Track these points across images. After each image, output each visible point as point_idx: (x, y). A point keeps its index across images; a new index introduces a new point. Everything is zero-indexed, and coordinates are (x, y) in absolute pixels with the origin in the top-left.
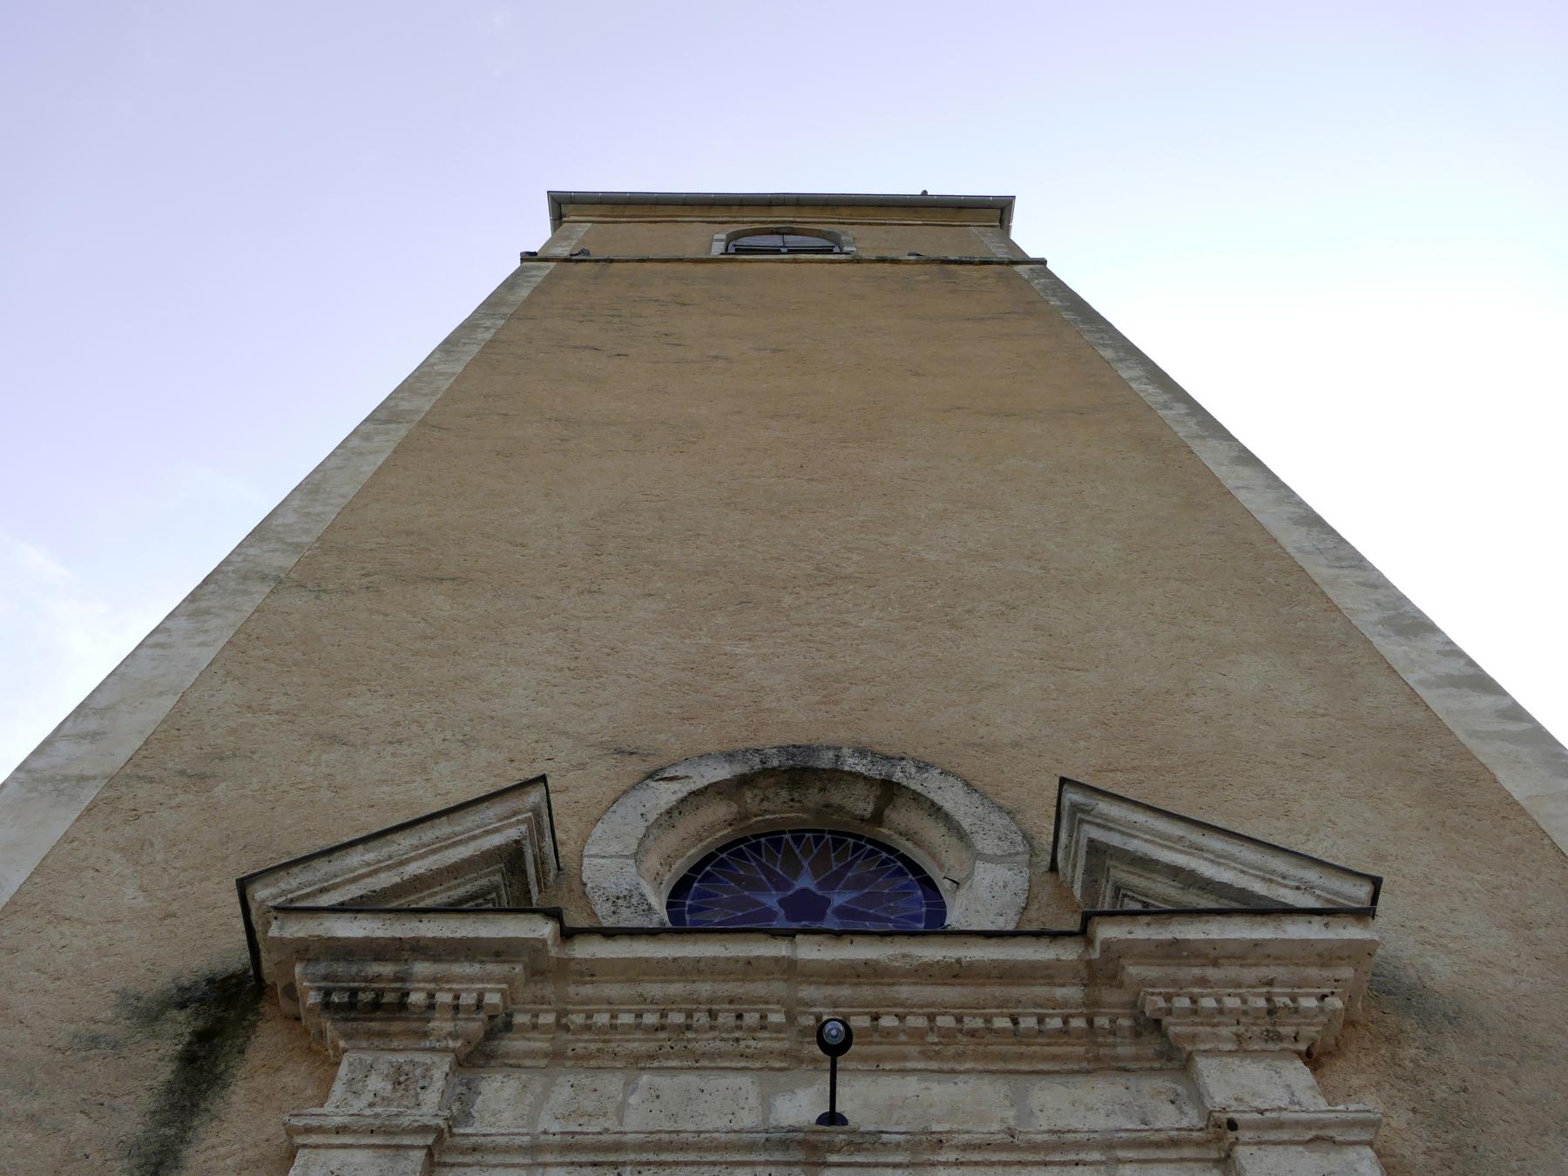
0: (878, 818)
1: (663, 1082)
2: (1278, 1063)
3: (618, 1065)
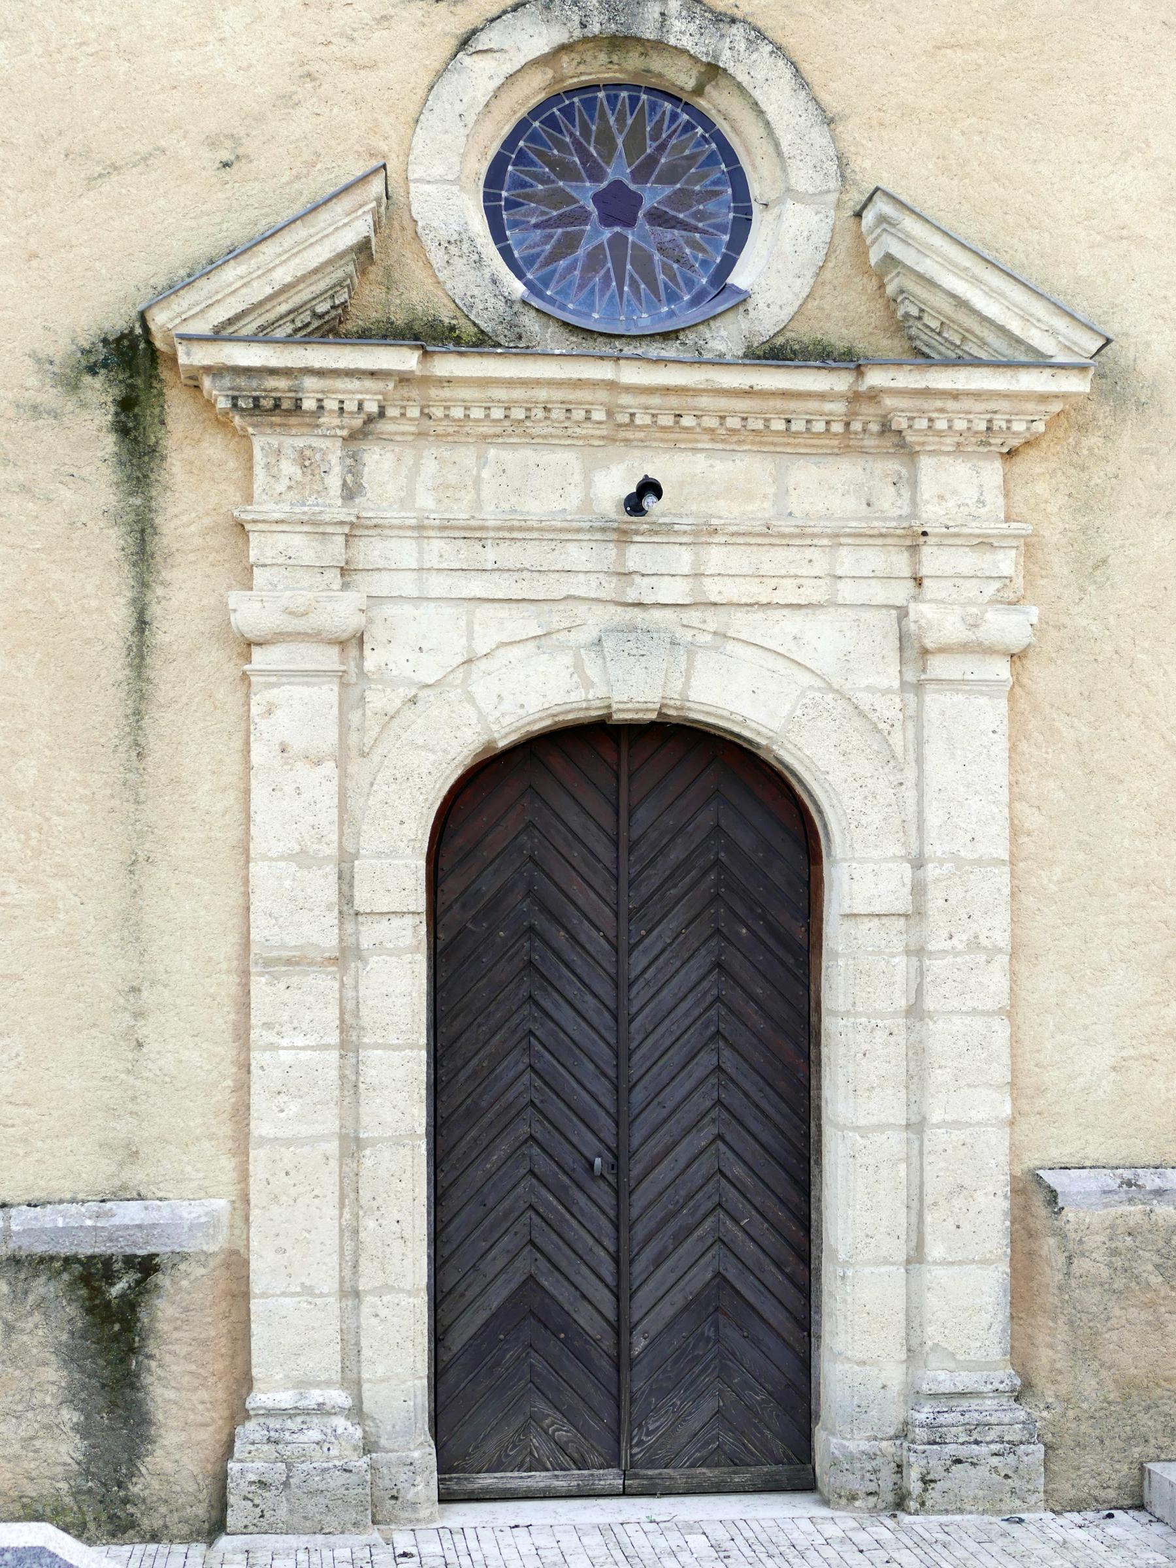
0: (699, 91)
1: (507, 456)
2: (981, 464)
3: (470, 440)
